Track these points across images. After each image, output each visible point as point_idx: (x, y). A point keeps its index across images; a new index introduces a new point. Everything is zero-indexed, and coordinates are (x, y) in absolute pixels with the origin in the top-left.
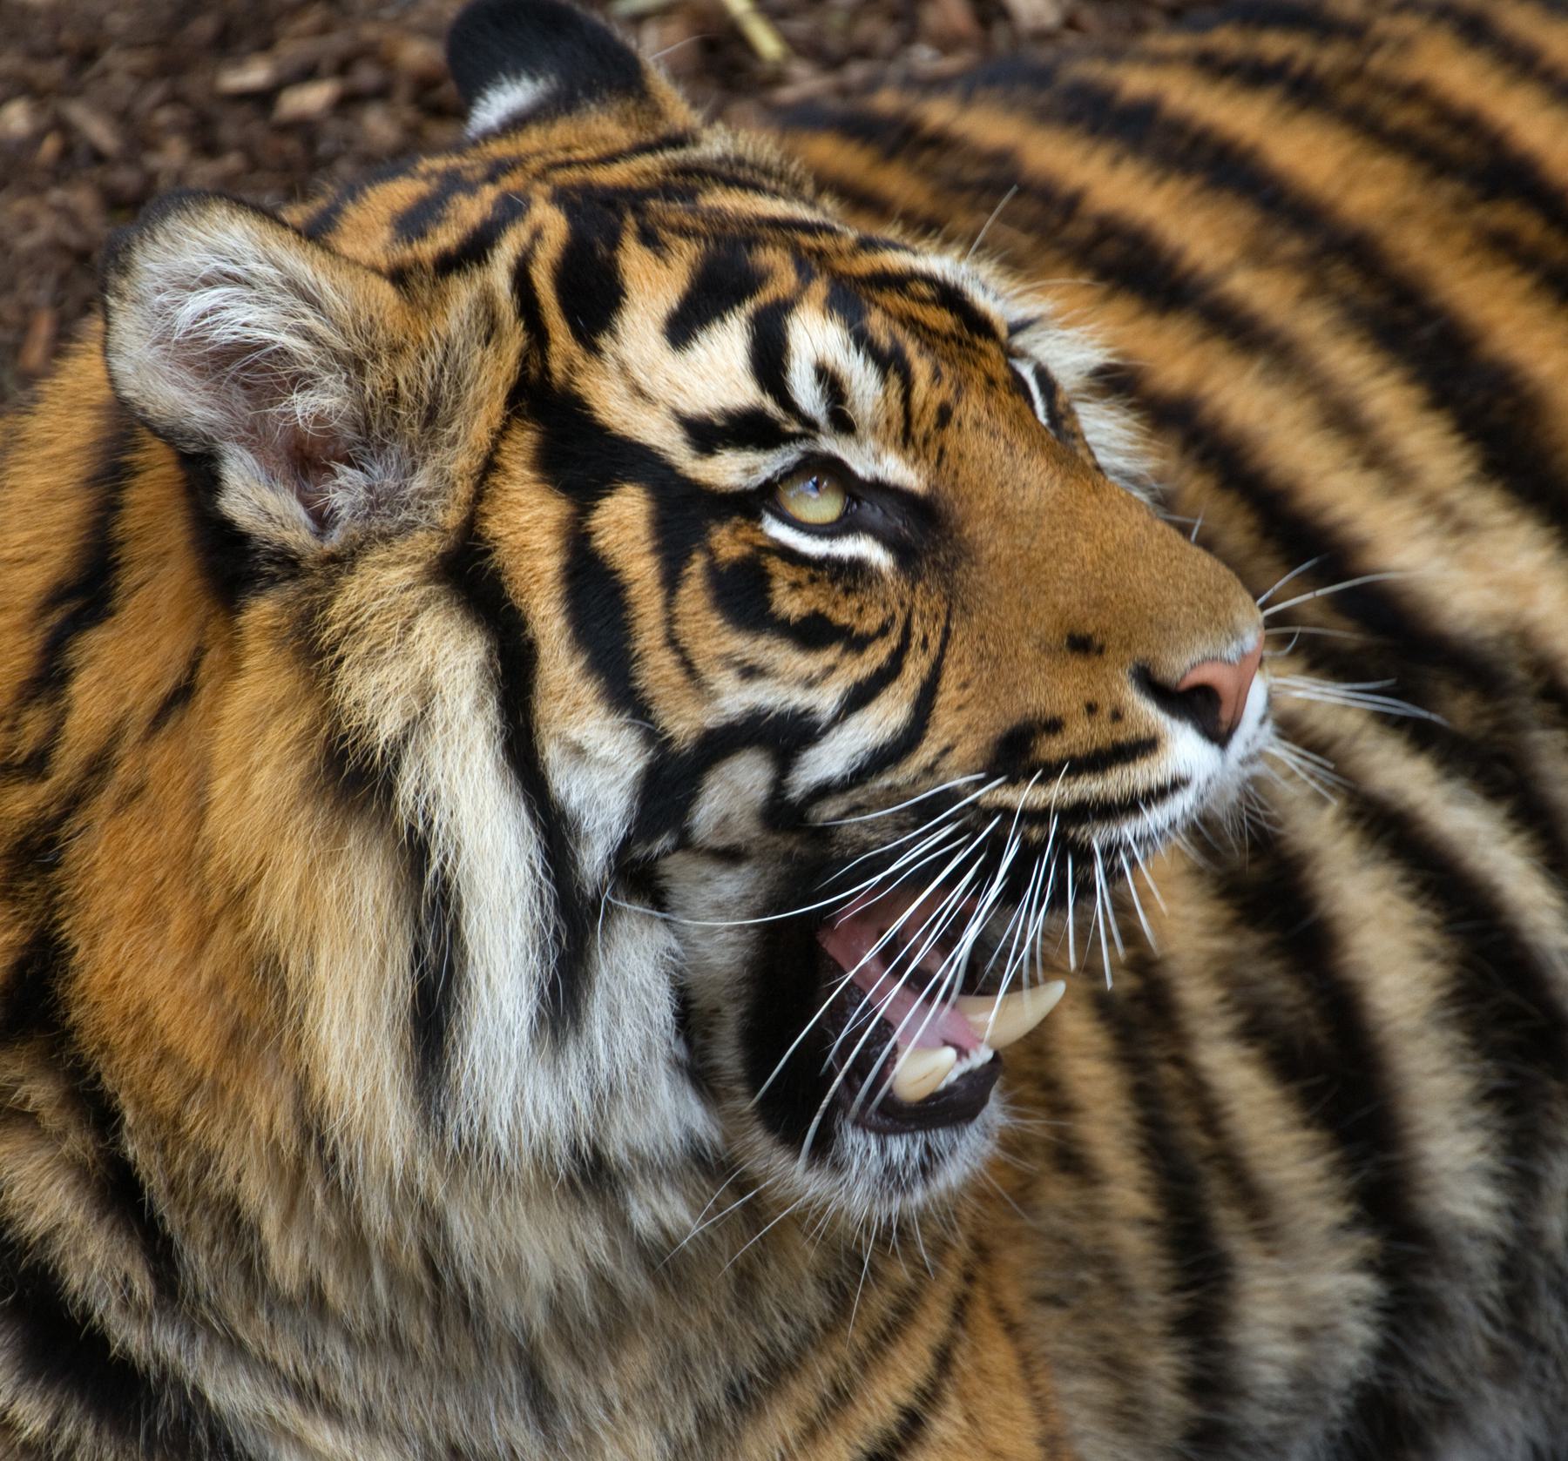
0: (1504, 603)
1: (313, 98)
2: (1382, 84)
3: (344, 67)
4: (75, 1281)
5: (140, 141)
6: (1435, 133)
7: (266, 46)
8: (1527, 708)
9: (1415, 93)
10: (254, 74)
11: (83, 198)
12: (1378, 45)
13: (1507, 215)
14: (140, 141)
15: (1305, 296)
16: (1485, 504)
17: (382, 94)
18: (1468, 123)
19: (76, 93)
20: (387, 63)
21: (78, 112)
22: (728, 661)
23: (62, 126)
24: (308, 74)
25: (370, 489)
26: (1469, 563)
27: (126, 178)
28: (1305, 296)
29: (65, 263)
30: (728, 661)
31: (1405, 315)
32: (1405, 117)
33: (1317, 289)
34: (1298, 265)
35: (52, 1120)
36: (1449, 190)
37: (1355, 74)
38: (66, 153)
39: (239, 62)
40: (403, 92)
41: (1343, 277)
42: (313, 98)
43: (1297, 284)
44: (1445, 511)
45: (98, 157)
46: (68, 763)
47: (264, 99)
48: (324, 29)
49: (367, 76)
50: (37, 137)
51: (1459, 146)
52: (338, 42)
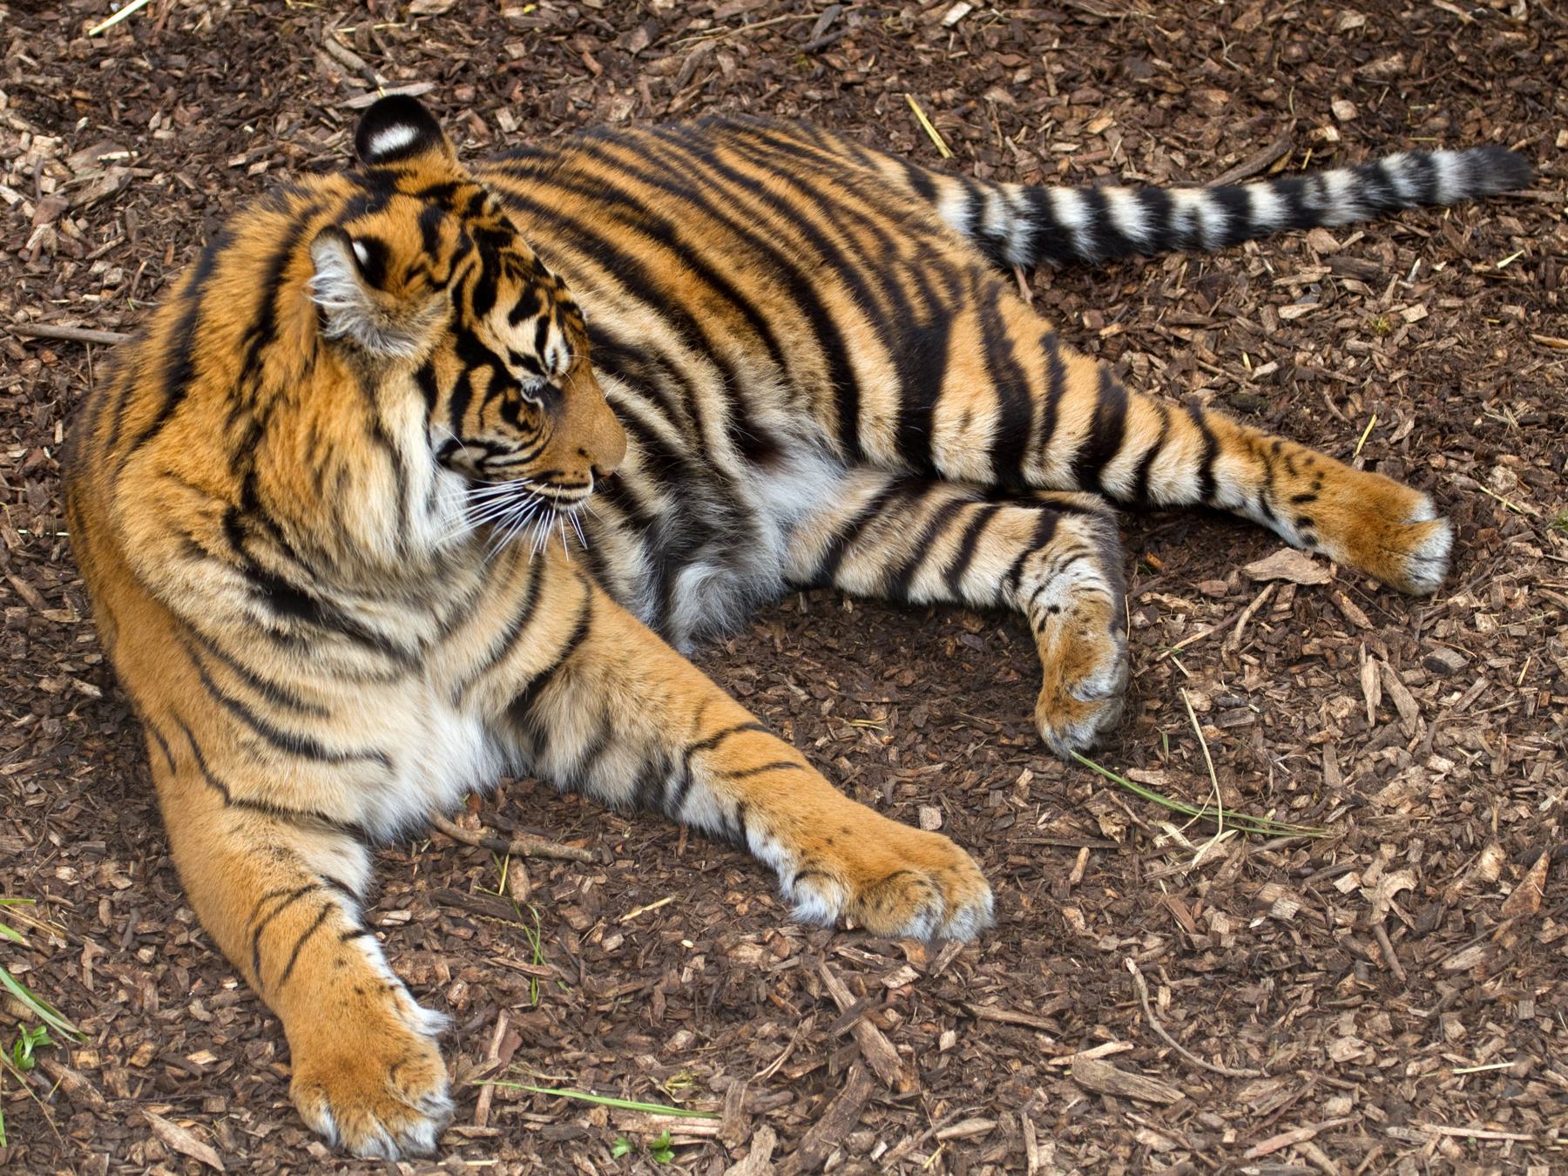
0: (642, 333)
1: (261, 167)
2: (565, 172)
3: (270, 156)
4: (288, 578)
5: (202, 185)
6: (589, 185)
7: (243, 151)
8: (654, 366)
9: (578, 174)
10: (241, 160)
11: (183, 206)
12: (563, 161)
13: (619, 209)
14: (202, 185)
15: (555, 238)
16: (629, 301)
17: (284, 164)
18: (599, 181)
19: (180, 170)
20: (285, 154)
21: (180, 176)
22: (495, 428)
23: (174, 181)
24: (259, 159)
25: (1127, 78)
26: (628, 321)
27: (197, 198)
28: (555, 238)
29: (179, 228)
30: (495, 428)
31: (590, 243)
32: (578, 181)
33: (558, 236)
34: (551, 229)
35: (266, 535)
36: (599, 202)
37: (556, 169)
38: (176, 190)
39: (235, 156)
40: (291, 165)
41: (567, 232)
42: (261, 167)
43: (552, 235)
44: (618, 304)
45: (188, 191)
46: (263, 398)
47: (244, 168)
48: (264, 143)
49: (279, 159)
50: (168, 185)
51: (597, 188)
52: (269, 147)
